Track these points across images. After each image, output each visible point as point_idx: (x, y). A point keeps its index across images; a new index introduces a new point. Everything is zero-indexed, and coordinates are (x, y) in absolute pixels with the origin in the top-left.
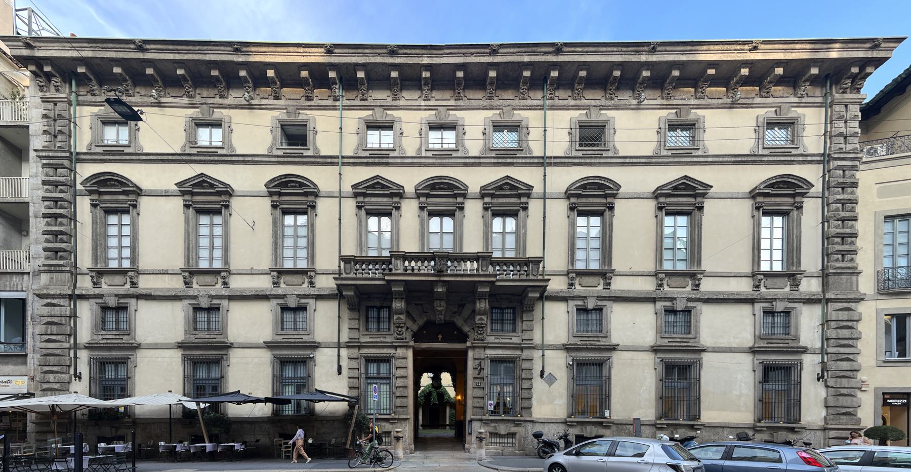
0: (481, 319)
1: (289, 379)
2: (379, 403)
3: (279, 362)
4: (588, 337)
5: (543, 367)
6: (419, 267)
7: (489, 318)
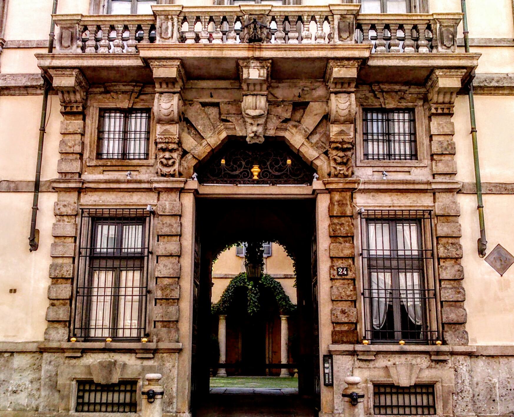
5: (482, 231)
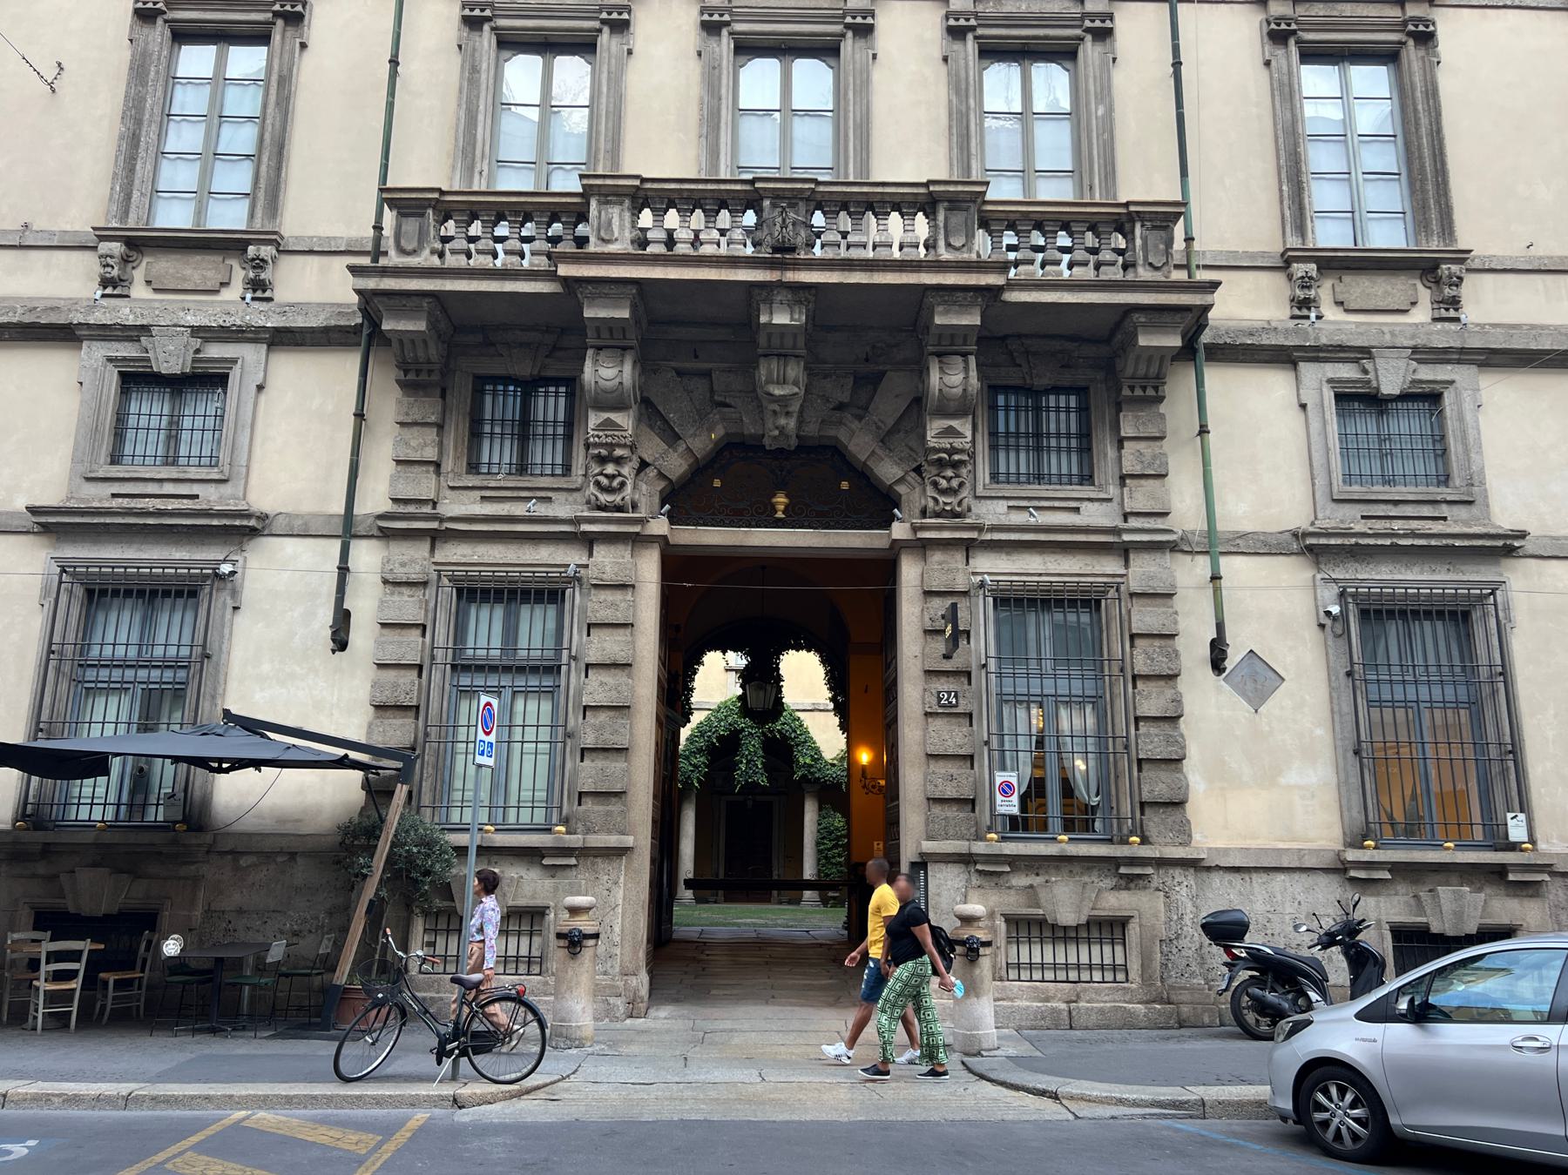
0: (950, 432)
1: (112, 664)
2: (500, 778)
3: (79, 591)
4: (1396, 503)
5: (1220, 627)
6: (697, 233)
7: (983, 429)
